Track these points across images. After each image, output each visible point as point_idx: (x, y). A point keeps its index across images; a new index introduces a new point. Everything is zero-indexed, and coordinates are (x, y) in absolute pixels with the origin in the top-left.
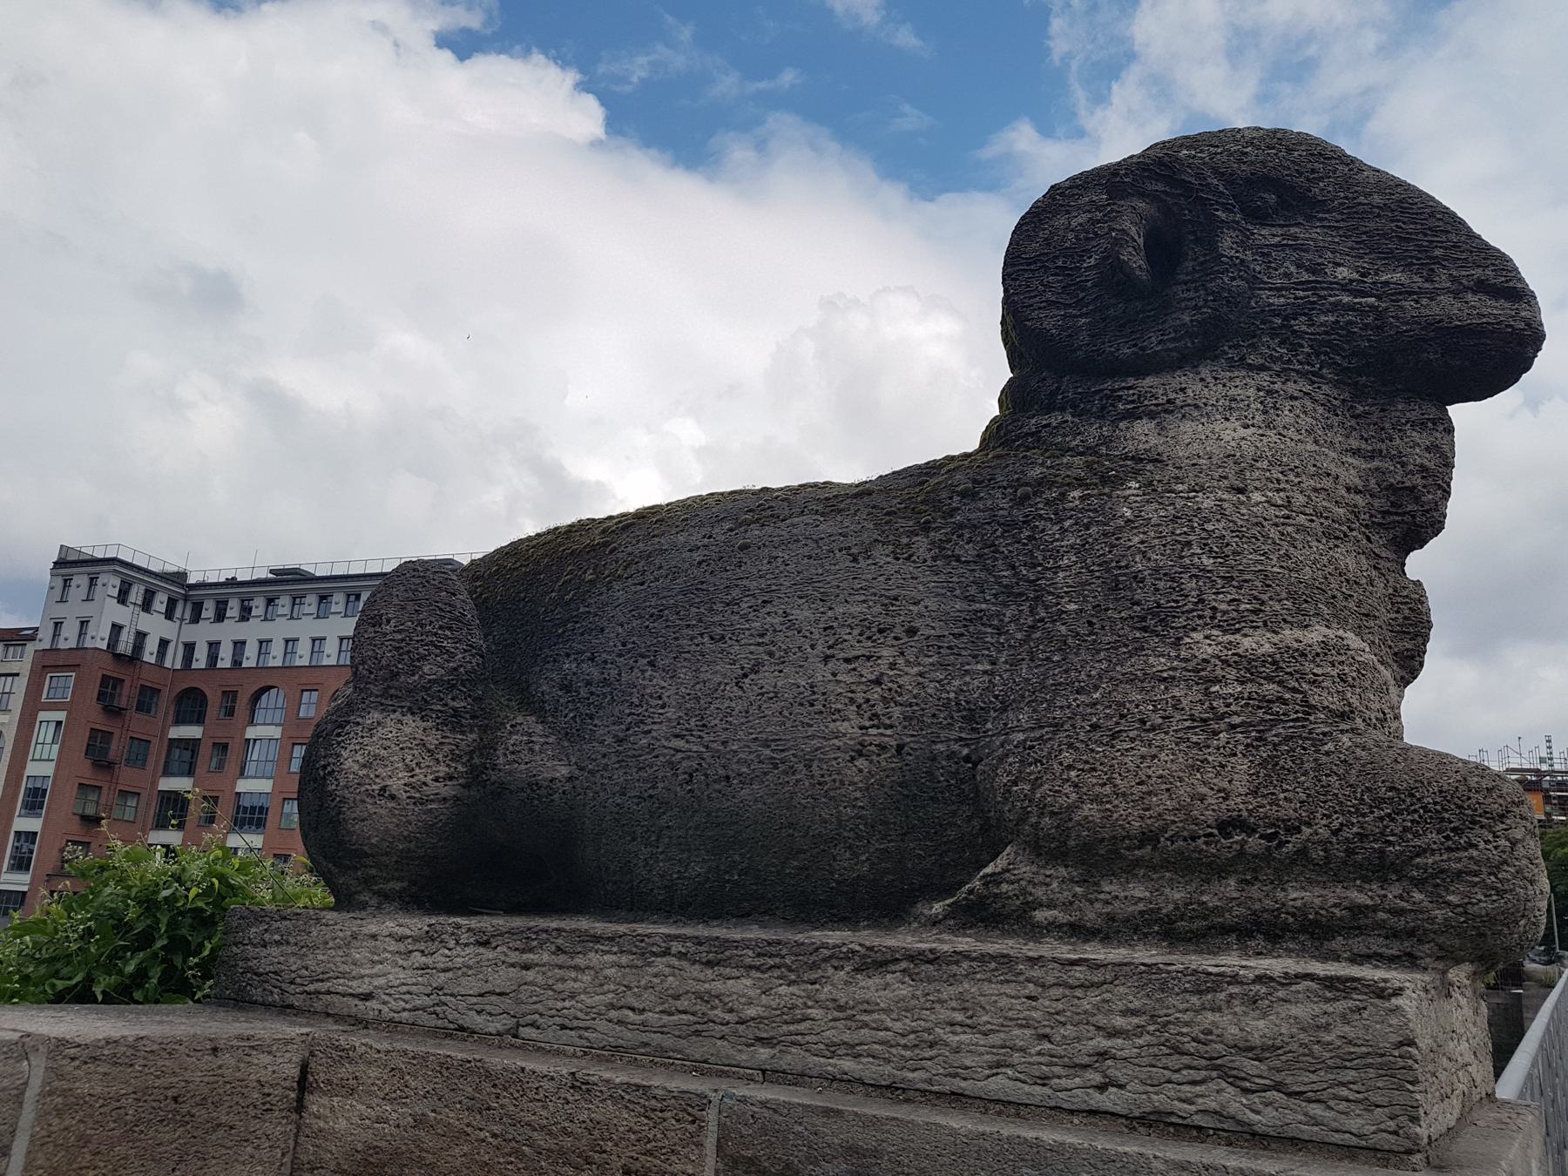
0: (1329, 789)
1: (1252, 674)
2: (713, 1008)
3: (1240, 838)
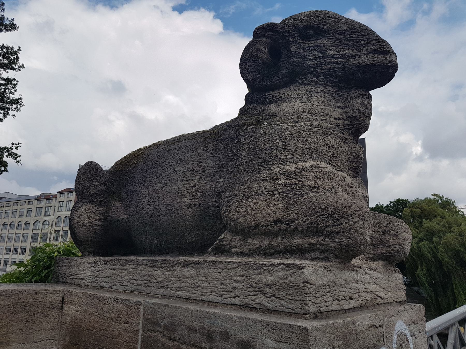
0: (303, 209)
1: (288, 177)
2: (152, 279)
3: (279, 225)
